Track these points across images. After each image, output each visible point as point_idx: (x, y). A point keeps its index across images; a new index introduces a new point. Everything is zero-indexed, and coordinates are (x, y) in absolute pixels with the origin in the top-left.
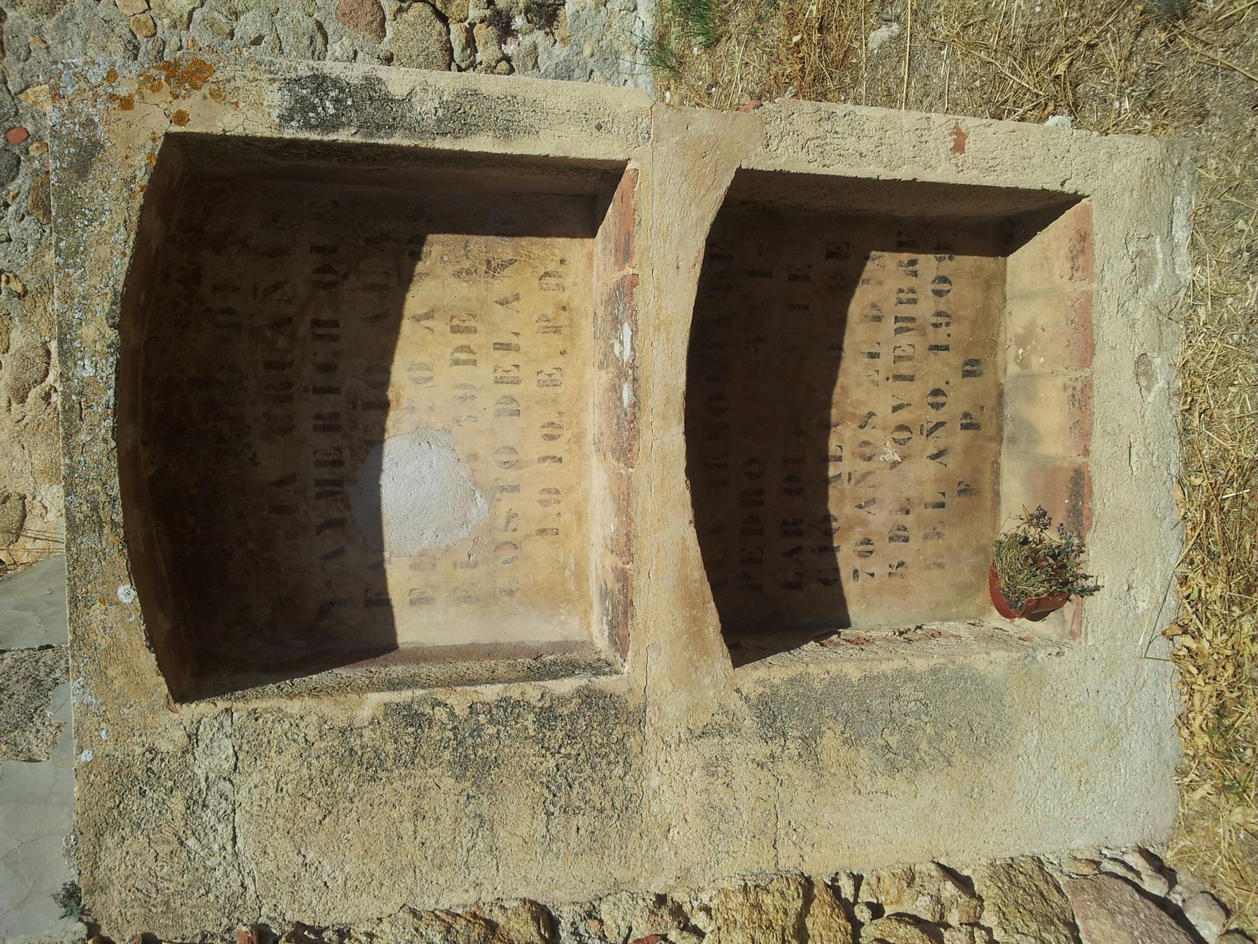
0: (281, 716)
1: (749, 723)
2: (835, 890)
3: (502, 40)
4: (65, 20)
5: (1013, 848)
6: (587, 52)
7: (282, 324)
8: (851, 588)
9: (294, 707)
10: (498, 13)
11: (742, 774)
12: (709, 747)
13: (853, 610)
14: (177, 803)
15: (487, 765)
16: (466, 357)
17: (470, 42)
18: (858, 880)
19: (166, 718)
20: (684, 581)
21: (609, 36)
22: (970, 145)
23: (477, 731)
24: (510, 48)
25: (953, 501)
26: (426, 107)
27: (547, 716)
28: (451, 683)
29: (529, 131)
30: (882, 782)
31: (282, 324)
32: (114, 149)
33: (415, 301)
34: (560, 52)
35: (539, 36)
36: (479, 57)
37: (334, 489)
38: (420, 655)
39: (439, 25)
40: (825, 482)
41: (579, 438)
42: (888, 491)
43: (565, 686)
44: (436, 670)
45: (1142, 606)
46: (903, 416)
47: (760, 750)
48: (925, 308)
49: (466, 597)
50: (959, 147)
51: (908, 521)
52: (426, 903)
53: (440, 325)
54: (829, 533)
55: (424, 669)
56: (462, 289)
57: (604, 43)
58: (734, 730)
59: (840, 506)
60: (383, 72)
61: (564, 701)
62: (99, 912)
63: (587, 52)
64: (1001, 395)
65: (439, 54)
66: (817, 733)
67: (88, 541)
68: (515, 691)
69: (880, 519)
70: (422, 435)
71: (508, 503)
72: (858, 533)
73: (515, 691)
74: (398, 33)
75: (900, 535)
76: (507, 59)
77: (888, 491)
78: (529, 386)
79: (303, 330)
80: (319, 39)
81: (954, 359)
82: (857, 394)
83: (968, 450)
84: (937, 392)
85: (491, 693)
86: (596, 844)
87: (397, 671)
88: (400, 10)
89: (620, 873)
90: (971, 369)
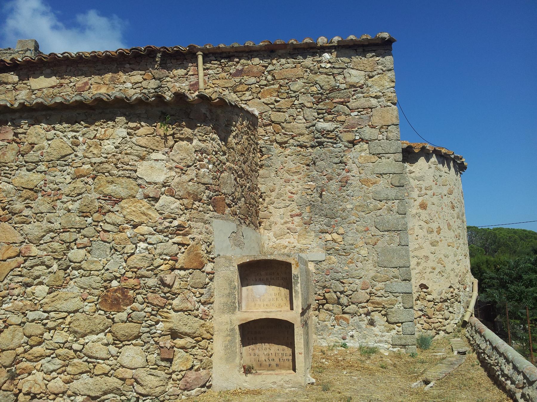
0: (236, 275)
1: (232, 327)
2: (212, 339)
3: (364, 314)
4: (356, 233)
5: (214, 365)
6: (365, 332)
7: (278, 274)
8: (248, 347)
9: (236, 276)
10: (370, 313)
11: (226, 326)
12: (229, 322)
13: (245, 348)
14: (228, 265)
15: (229, 296)
16: (275, 295)
17: (363, 307)
18: (212, 342)
19: (236, 264)
20: (248, 318)
21: (369, 337)
22: (300, 355)
23: (233, 295)
24: (363, 315)
25: (259, 363)
26: (297, 288)
27: (234, 303)
28: (238, 292)
29: (295, 299)
30: (224, 345)
31: (278, 274)
32: (289, 258)
33: (281, 288)
34: (364, 326)
35: (366, 322)
36: (360, 309)
37: (260, 280)
38: (241, 290)
39: (365, 301)
40: (262, 343)
41: (266, 309)
42: (261, 353)
43: (237, 305)
44: (239, 291)
45: (244, 384)
46: (270, 355)
47: (228, 329)
48: (285, 358)
49: (248, 296)
50: (300, 354)
51: (257, 356)
52: (215, 290)
53: (279, 291)
54: (255, 344)
55: (240, 290)
56: (283, 294)
57: (367, 336)
58: (231, 326)
59: (259, 345)
60: (300, 284)
61: (235, 305)
62: (217, 258)
63: (365, 332)
64: (274, 370)
65: (359, 301)
66: (230, 336)
67: (253, 257)
68: (237, 299)
69: (257, 351)
70: (266, 290)
71: (259, 300)
72: (255, 348)
73: (237, 299)
74: (362, 293)
75: (255, 355)
76: (361, 315)
77: (261, 353)
78: (272, 302)
79: (277, 276)
80: (359, 278)
81: (278, 363)
82: (273, 348)
83: (266, 365)
84: (274, 360)
85: (237, 296)
86: (220, 309)
87: (240, 287)
88: (367, 293)
89: (216, 312)
90: (277, 365)
